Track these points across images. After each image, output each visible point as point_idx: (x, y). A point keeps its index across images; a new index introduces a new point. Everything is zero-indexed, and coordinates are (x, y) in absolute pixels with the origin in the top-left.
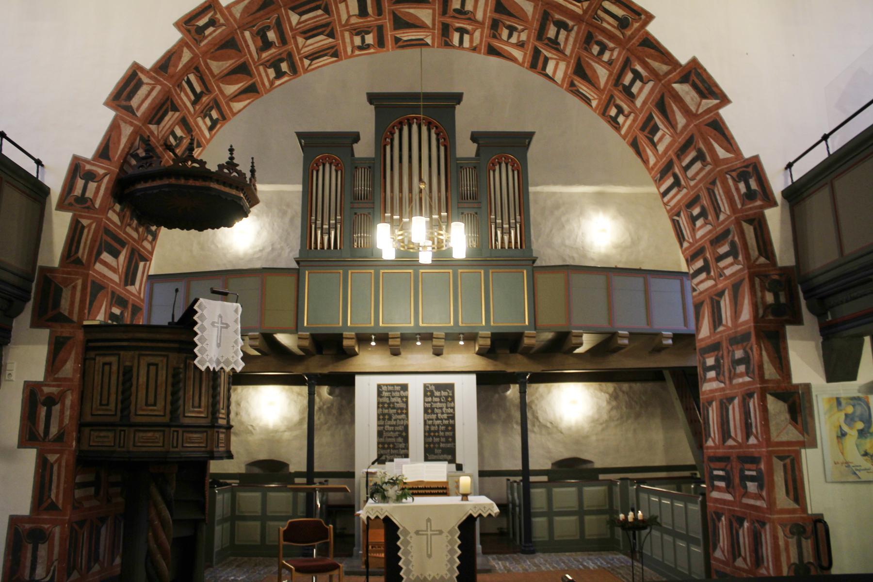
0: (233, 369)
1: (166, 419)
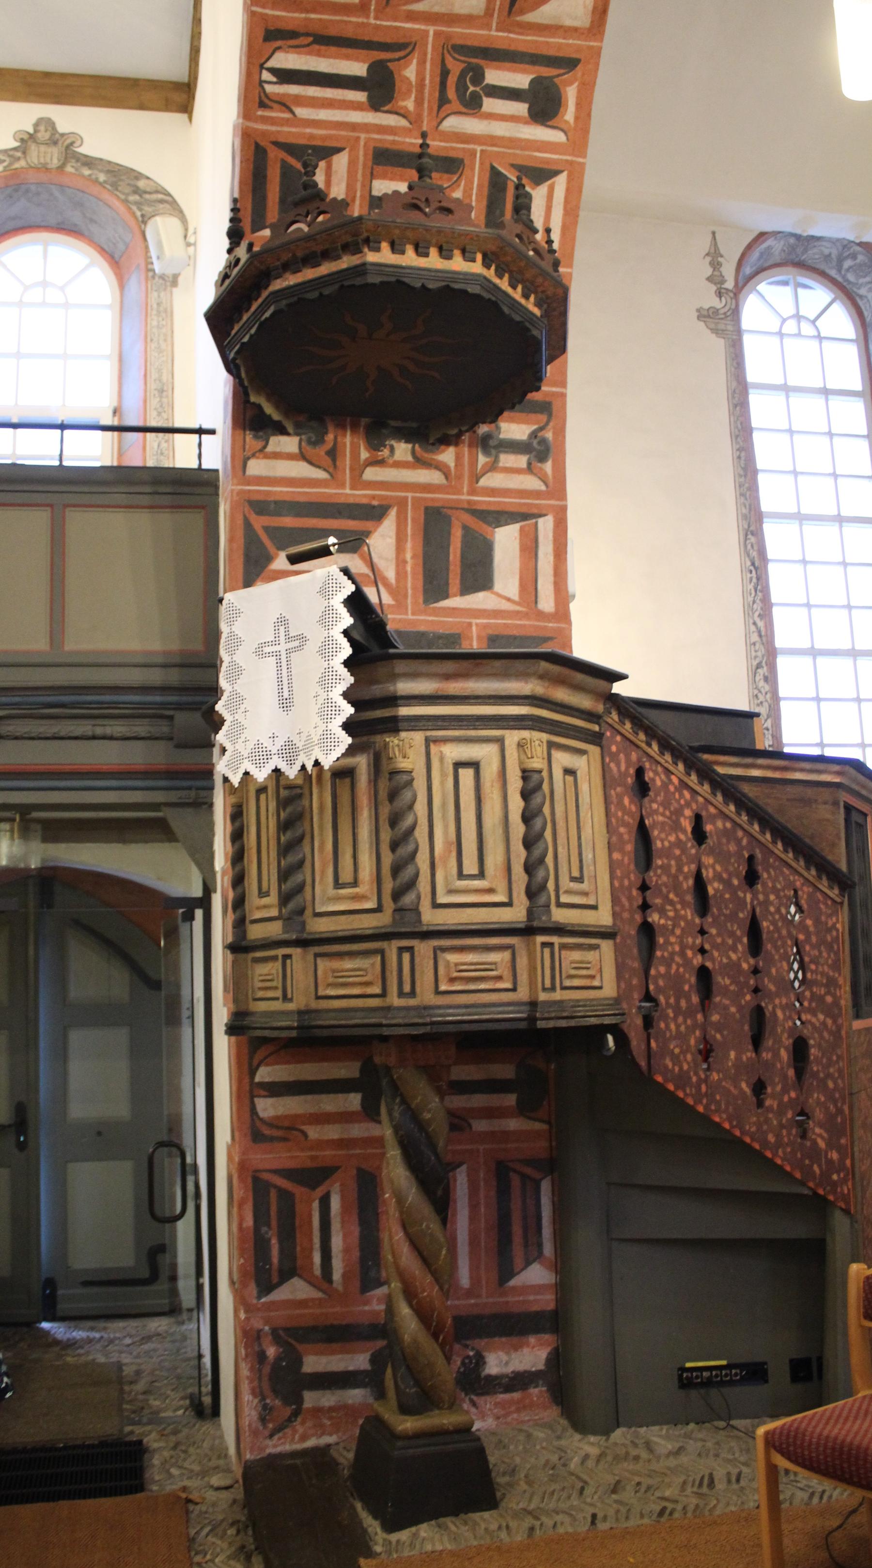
0: (277, 771)
1: (516, 914)
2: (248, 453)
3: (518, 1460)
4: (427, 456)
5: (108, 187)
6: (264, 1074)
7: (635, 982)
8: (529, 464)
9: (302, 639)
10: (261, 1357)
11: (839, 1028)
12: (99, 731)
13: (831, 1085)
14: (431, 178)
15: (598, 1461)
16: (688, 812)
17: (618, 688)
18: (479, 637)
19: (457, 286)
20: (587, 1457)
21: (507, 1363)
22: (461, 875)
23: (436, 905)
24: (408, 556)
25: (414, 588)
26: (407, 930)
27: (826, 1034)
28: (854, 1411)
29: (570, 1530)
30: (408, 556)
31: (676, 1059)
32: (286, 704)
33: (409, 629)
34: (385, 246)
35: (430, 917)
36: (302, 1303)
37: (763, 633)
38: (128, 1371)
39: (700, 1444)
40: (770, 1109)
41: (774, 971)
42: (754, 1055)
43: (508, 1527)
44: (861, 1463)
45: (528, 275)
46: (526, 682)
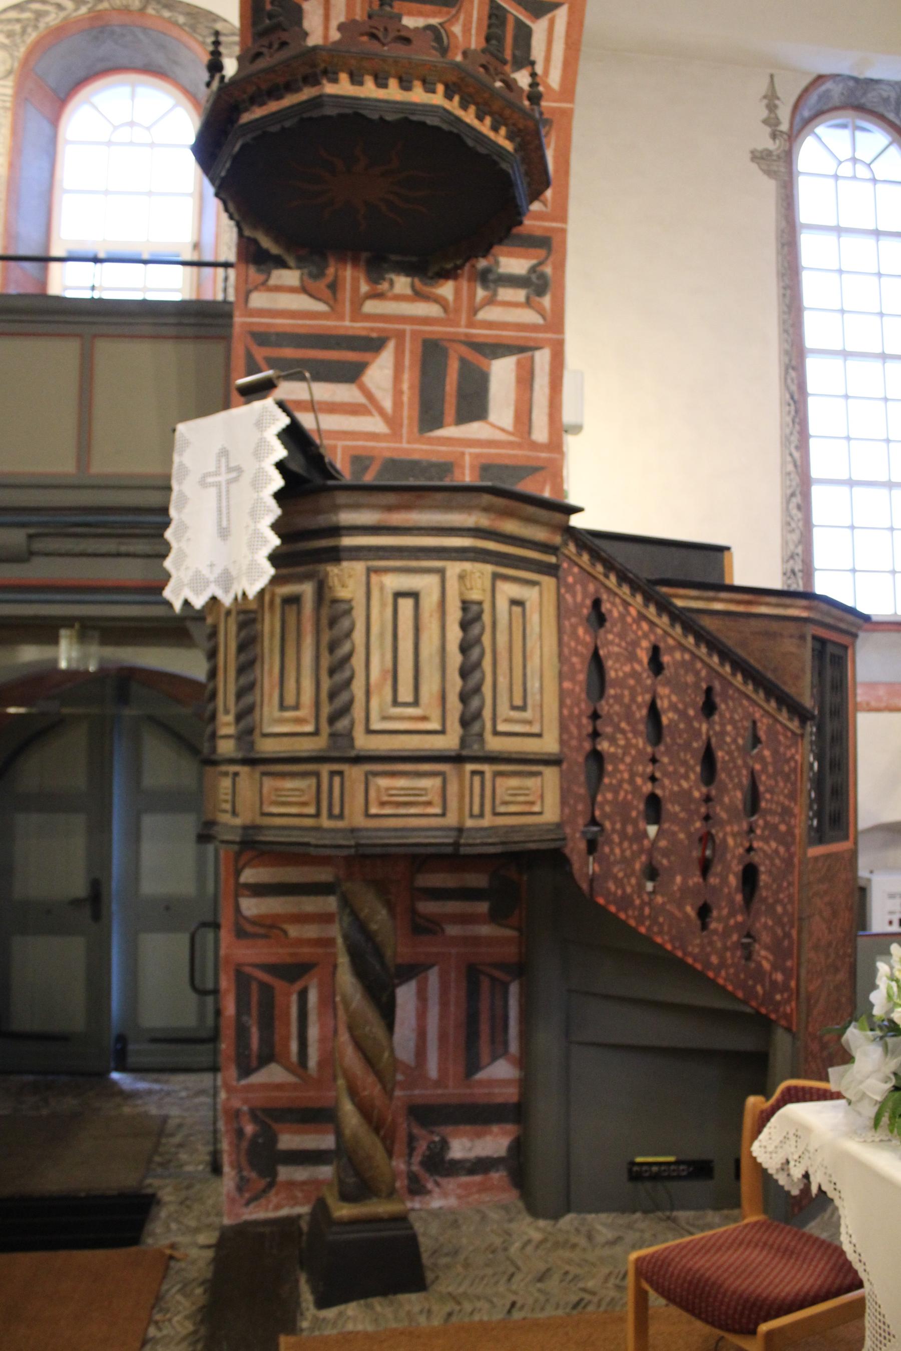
1: (450, 742)
2: (250, 287)
3: (464, 1241)
4: (427, 289)
5: (187, 29)
6: (249, 876)
7: (580, 807)
8: (528, 298)
9: (239, 470)
10: (240, 1133)
11: (791, 856)
12: (123, 549)
13: (779, 909)
14: (391, 6)
15: (537, 1247)
16: (645, 644)
17: (576, 521)
18: (472, 467)
19: (415, 118)
20: (529, 1241)
21: (470, 1149)
22: (395, 703)
23: (369, 731)
24: (405, 386)
25: (410, 418)
26: (341, 754)
27: (777, 862)
28: (729, 1241)
29: (485, 1318)
30: (405, 386)
31: (619, 883)
32: (224, 533)
33: (403, 457)
34: (344, 77)
35: (363, 742)
36: (279, 1087)
37: (799, 463)
38: (172, 1123)
39: (638, 1235)
40: (715, 931)
41: (726, 800)
42: (701, 880)
43: (429, 1311)
44: (711, 1300)
45: (496, 106)
46: (470, 514)
